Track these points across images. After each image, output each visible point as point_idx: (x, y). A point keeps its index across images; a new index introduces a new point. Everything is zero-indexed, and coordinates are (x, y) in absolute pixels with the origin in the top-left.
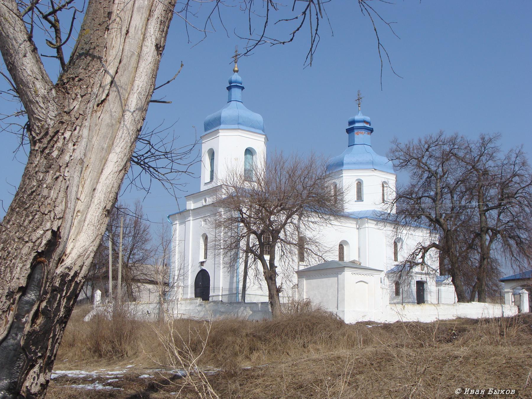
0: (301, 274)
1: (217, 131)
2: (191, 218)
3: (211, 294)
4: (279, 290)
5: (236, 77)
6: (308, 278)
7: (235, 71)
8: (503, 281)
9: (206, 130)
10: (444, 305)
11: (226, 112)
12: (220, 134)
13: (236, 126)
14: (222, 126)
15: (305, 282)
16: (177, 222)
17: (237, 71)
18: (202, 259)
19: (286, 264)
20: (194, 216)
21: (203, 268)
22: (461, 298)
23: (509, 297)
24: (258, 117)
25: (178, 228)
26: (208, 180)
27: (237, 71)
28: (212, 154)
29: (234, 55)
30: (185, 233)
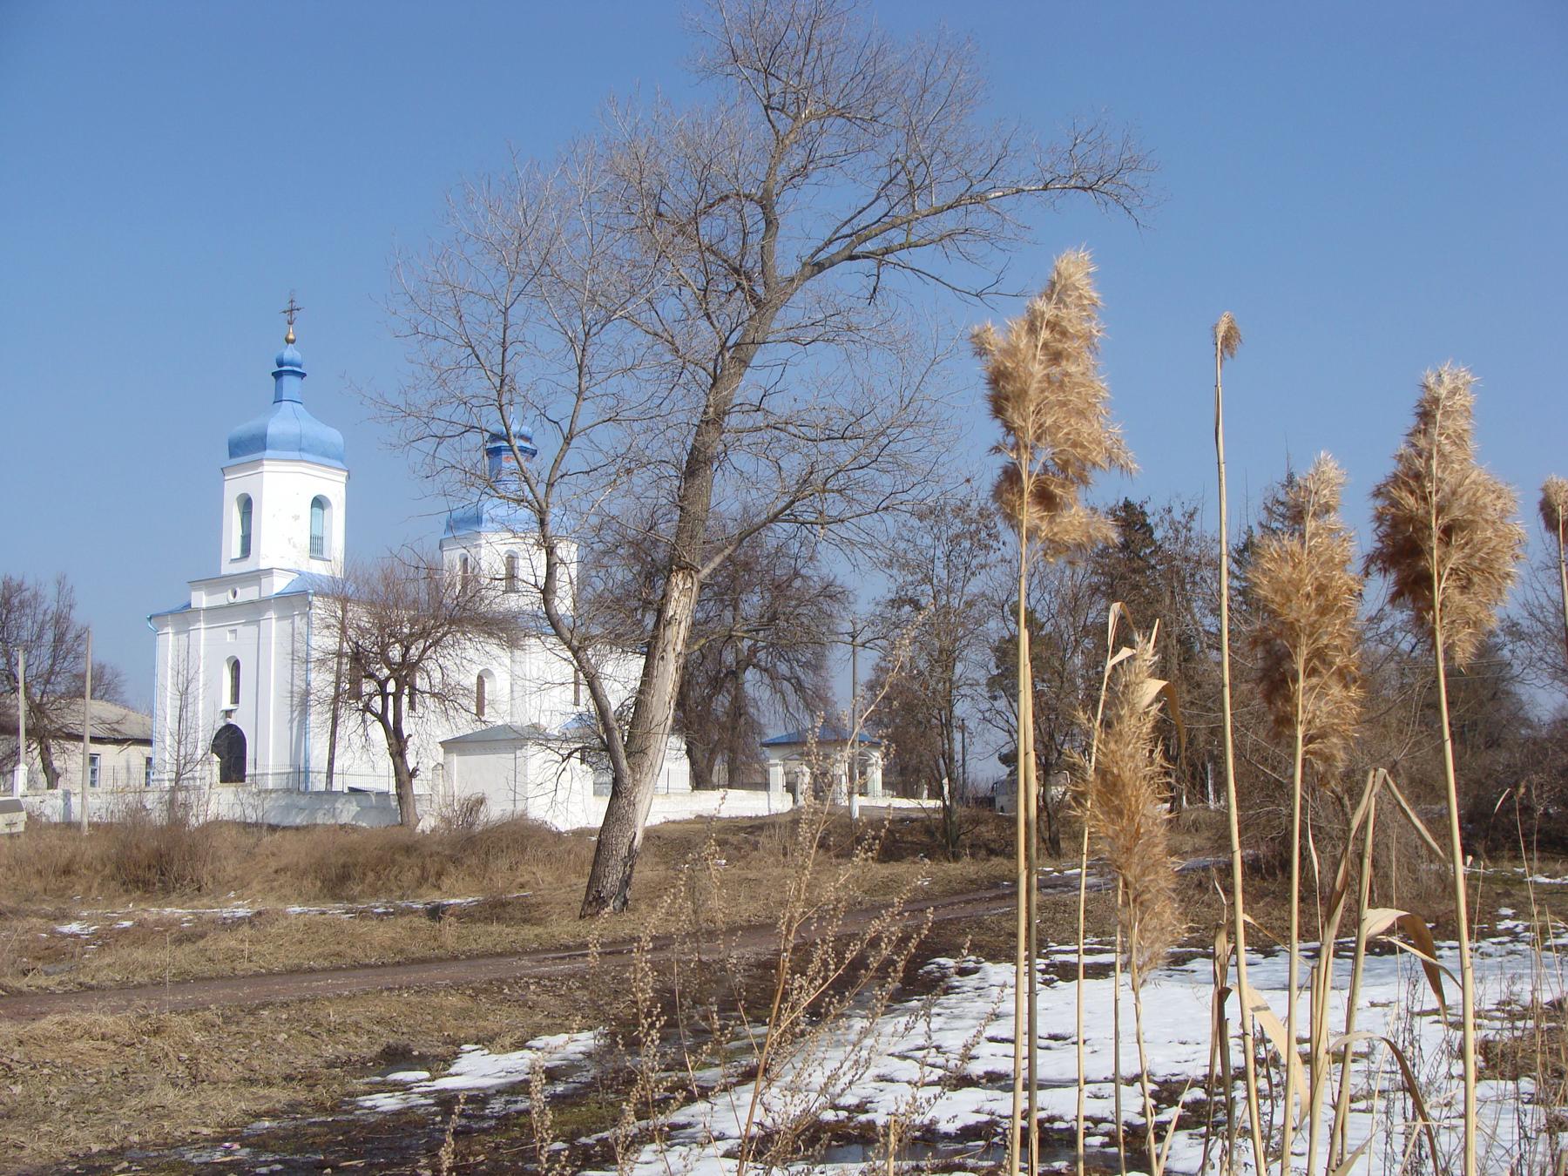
0: (450, 746)
1: (259, 462)
2: (202, 625)
3: (249, 770)
4: (413, 774)
5: (290, 353)
6: (462, 753)
7: (288, 341)
8: (768, 745)
9: (232, 454)
10: (670, 795)
11: (280, 424)
12: (266, 468)
13: (296, 455)
14: (268, 453)
15: (455, 759)
16: (170, 630)
17: (293, 342)
18: (227, 704)
19: (427, 729)
20: (207, 621)
21: (232, 721)
22: (700, 780)
23: (777, 774)
24: (334, 436)
25: (169, 642)
26: (237, 553)
27: (293, 342)
28: (246, 504)
29: (288, 307)
30: (187, 656)
